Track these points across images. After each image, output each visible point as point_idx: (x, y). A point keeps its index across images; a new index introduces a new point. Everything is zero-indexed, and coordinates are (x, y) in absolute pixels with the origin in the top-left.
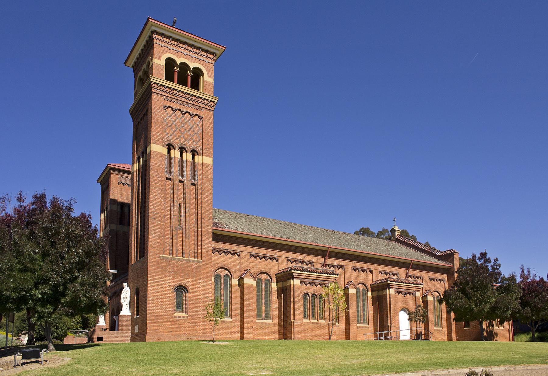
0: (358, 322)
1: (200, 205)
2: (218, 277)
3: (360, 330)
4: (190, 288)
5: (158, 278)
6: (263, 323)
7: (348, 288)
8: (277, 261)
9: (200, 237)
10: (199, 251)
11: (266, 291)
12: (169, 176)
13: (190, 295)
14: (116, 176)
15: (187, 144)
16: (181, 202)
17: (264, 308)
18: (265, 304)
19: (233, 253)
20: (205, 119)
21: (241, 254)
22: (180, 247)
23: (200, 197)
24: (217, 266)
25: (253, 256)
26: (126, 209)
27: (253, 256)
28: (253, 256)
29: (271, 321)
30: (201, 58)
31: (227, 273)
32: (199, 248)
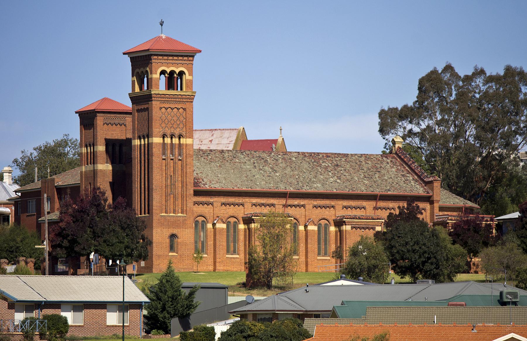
0: (319, 254)
1: (185, 175)
2: (197, 223)
3: (320, 262)
4: (179, 235)
5: (159, 230)
6: (231, 258)
7: (307, 226)
8: (243, 206)
9: (185, 198)
10: (185, 208)
11: (235, 232)
12: (164, 158)
13: (179, 240)
14: (101, 118)
15: (175, 132)
16: (172, 174)
17: (232, 245)
18: (233, 242)
19: (208, 204)
20: (187, 110)
21: (214, 204)
22: (172, 207)
23: (185, 169)
24: (196, 215)
25: (224, 204)
26: (124, 149)
27: (223, 204)
28: (223, 204)
29: (238, 256)
30: (184, 62)
31: (203, 219)
32: (185, 206)
